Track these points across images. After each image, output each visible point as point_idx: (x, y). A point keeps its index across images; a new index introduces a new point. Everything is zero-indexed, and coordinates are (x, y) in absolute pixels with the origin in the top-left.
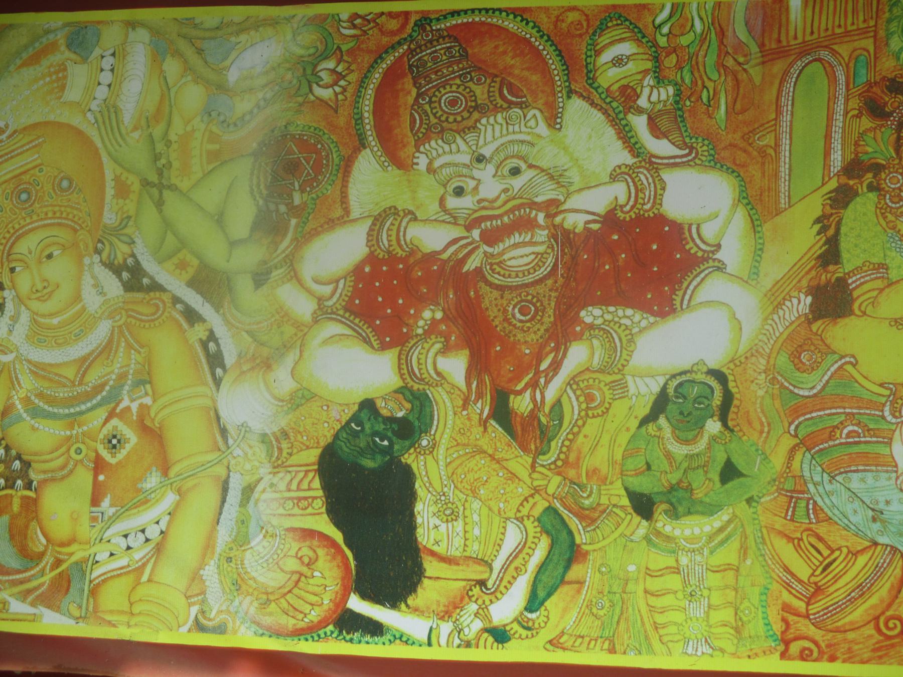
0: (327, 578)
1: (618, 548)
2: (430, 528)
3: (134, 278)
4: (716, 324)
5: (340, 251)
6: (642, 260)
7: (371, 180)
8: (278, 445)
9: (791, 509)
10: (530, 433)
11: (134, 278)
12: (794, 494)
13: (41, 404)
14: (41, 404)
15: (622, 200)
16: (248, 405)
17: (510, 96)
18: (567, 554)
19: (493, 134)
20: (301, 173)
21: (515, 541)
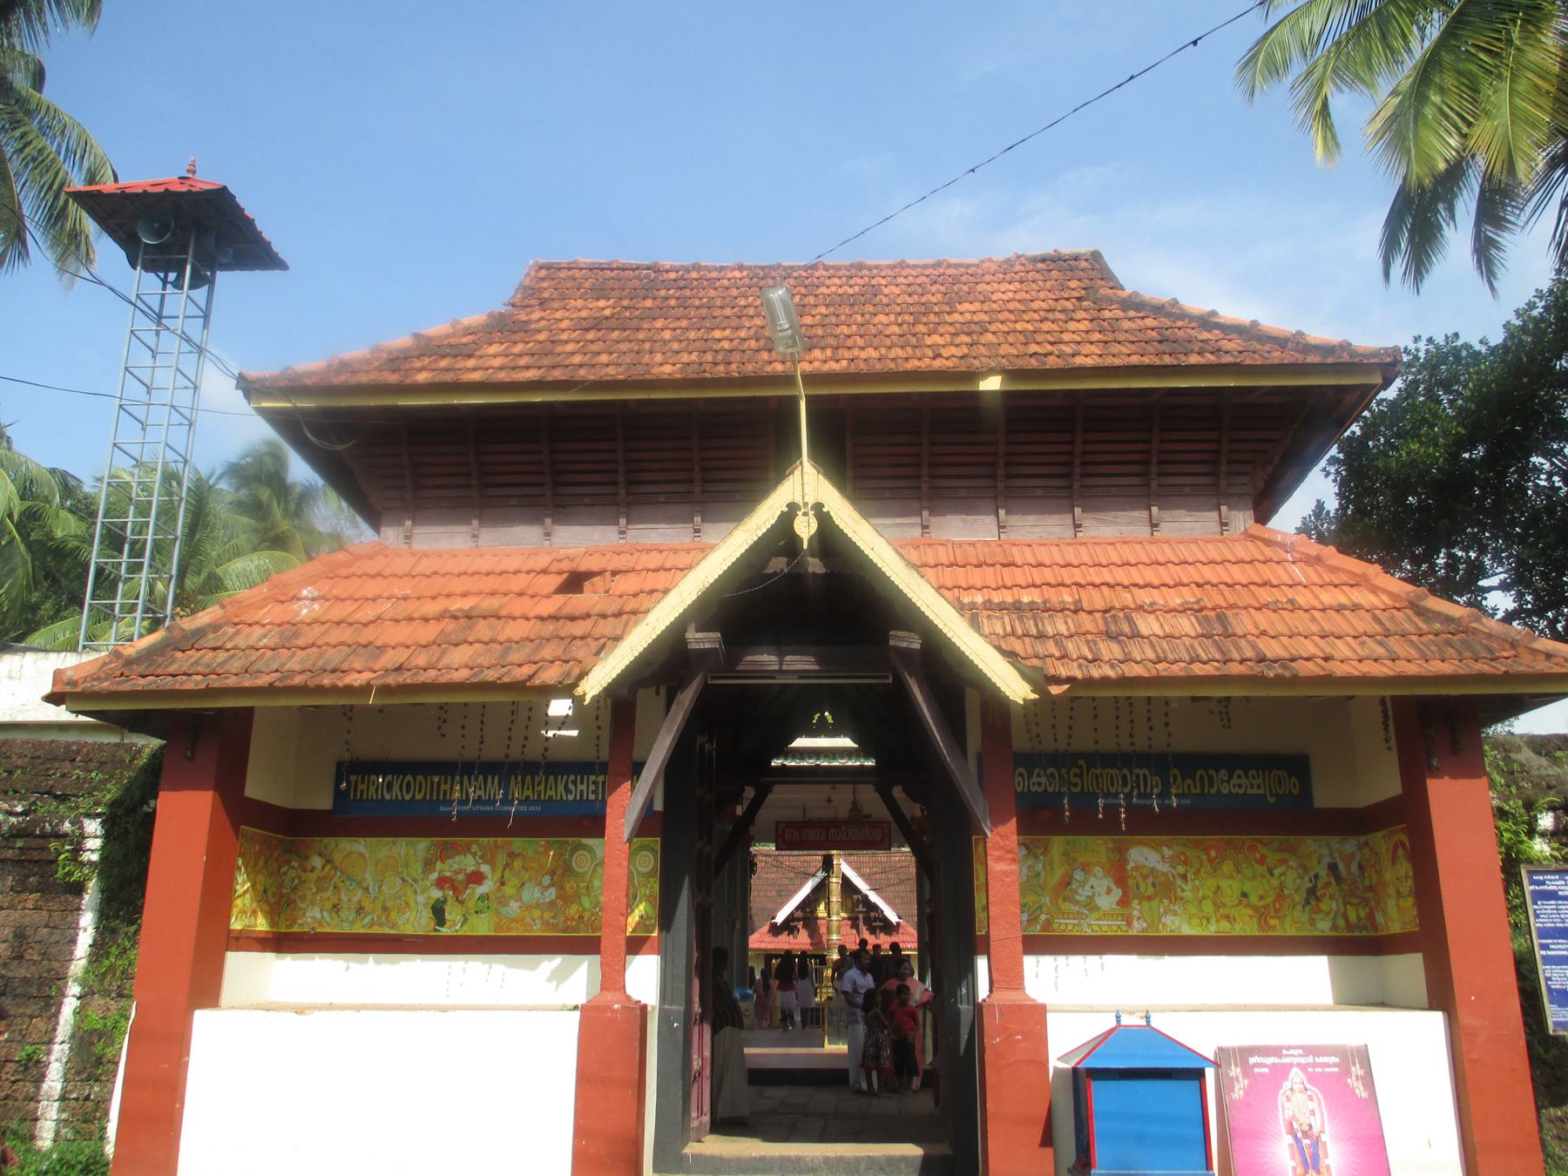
0: (433, 923)
1: (473, 919)
2: (447, 916)
3: (403, 880)
4: (485, 888)
5: (434, 876)
6: (477, 878)
7: (439, 865)
8: (425, 905)
9: (1481, 56)
10: (462, 903)
11: (403, 880)
12: (497, 911)
13: (54, 1082)
14: (54, 1082)
15: (40, 1143)
16: (421, 899)
17: (459, 853)
18: (466, 919)
19: (457, 858)
20: (428, 865)
21: (459, 918)
